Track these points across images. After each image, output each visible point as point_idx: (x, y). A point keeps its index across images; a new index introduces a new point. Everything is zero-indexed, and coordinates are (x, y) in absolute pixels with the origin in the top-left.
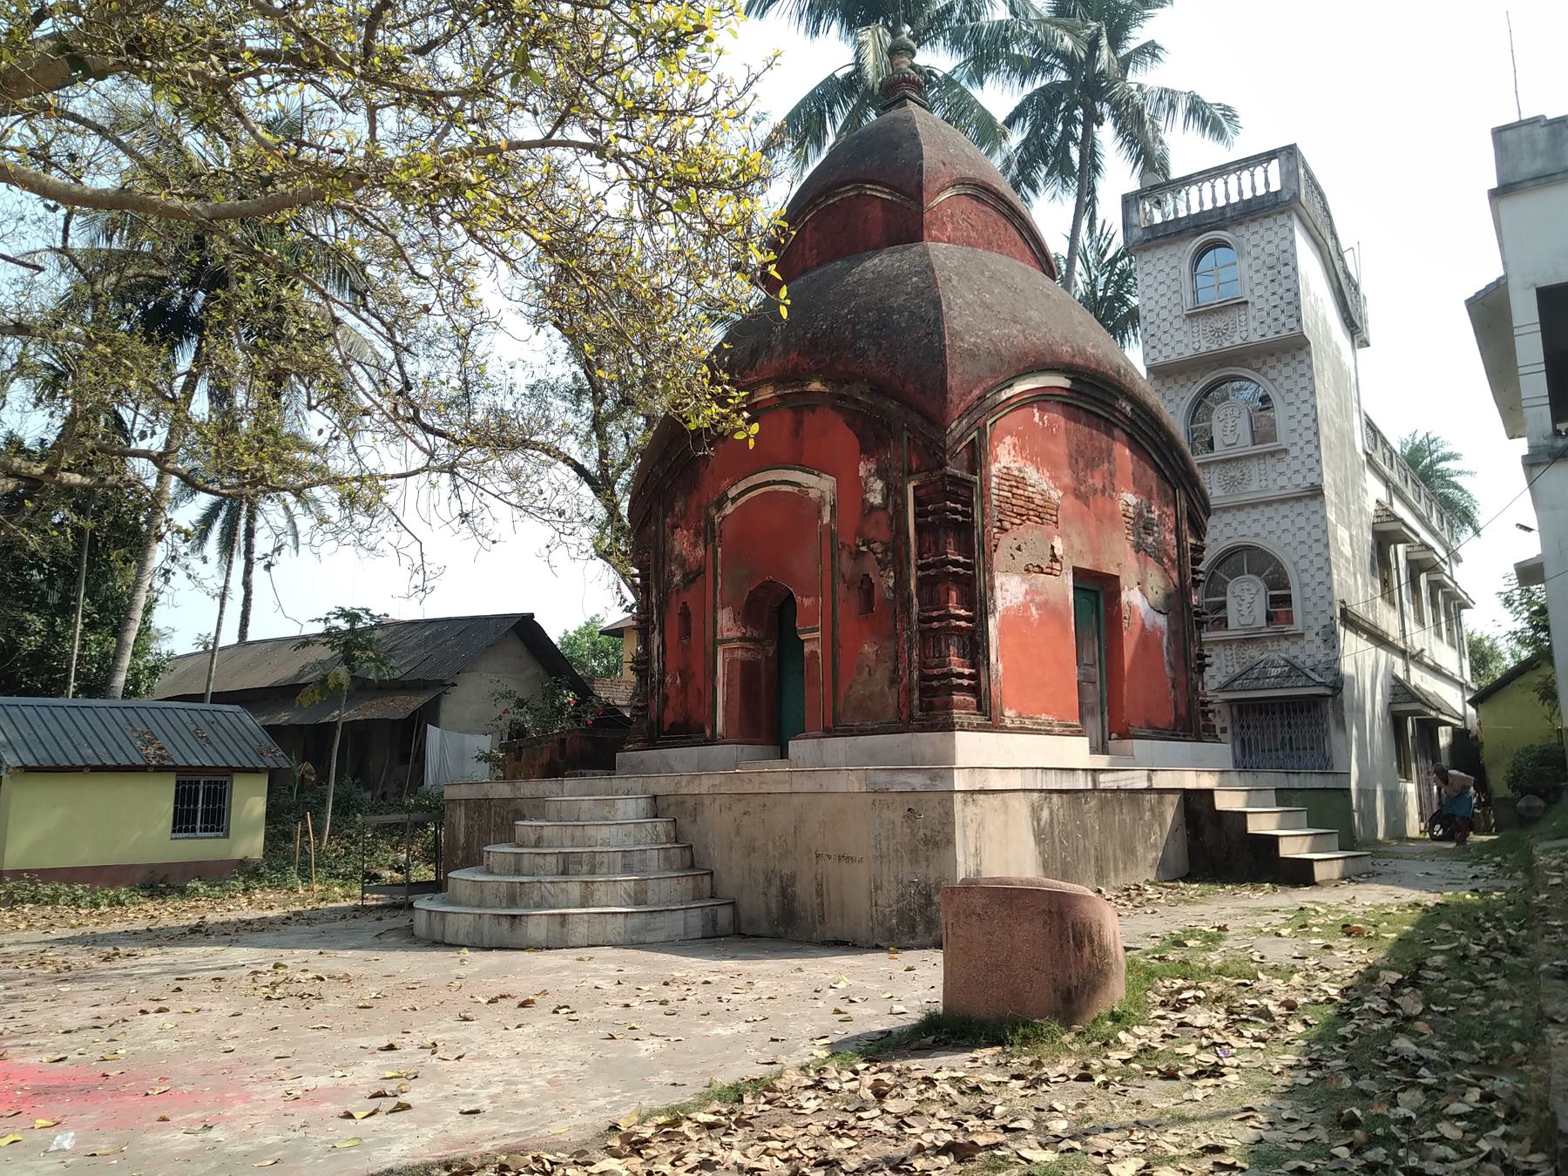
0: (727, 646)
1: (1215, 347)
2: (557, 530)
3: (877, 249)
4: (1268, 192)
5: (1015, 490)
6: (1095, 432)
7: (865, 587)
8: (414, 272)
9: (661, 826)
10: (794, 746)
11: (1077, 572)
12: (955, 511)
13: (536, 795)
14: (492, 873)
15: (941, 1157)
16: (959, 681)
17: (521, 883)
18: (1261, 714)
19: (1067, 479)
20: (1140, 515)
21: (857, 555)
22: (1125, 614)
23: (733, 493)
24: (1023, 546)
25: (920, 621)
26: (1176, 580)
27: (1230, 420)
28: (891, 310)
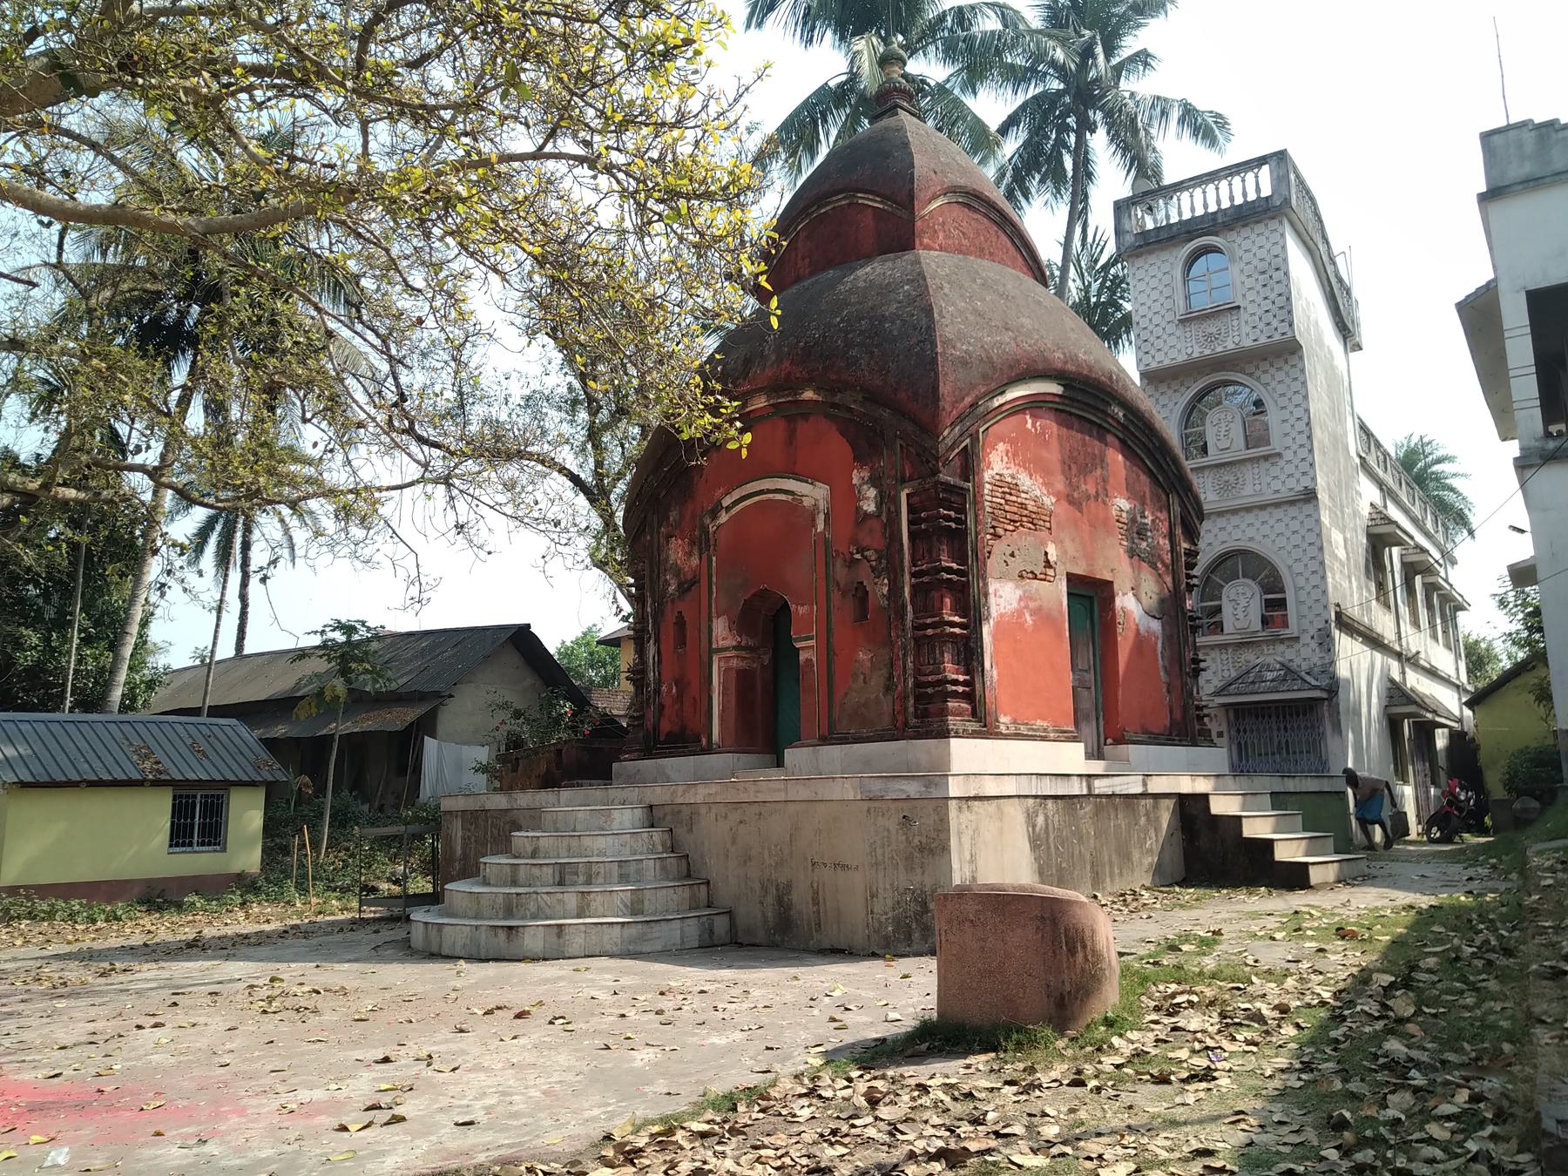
1: (1207, 352)
2: (553, 540)
3: (868, 257)
5: (1008, 497)
7: (860, 594)
8: (407, 285)
9: (657, 836)
10: (790, 755)
11: (1071, 578)
12: (949, 518)
16: (954, 688)
17: (518, 894)
18: (1257, 717)
19: (1060, 484)
20: (1133, 520)
21: (851, 563)
22: (1120, 619)
23: (727, 502)
24: (1016, 553)
25: (915, 628)
26: (1170, 585)
27: (1223, 425)
28: (883, 318)
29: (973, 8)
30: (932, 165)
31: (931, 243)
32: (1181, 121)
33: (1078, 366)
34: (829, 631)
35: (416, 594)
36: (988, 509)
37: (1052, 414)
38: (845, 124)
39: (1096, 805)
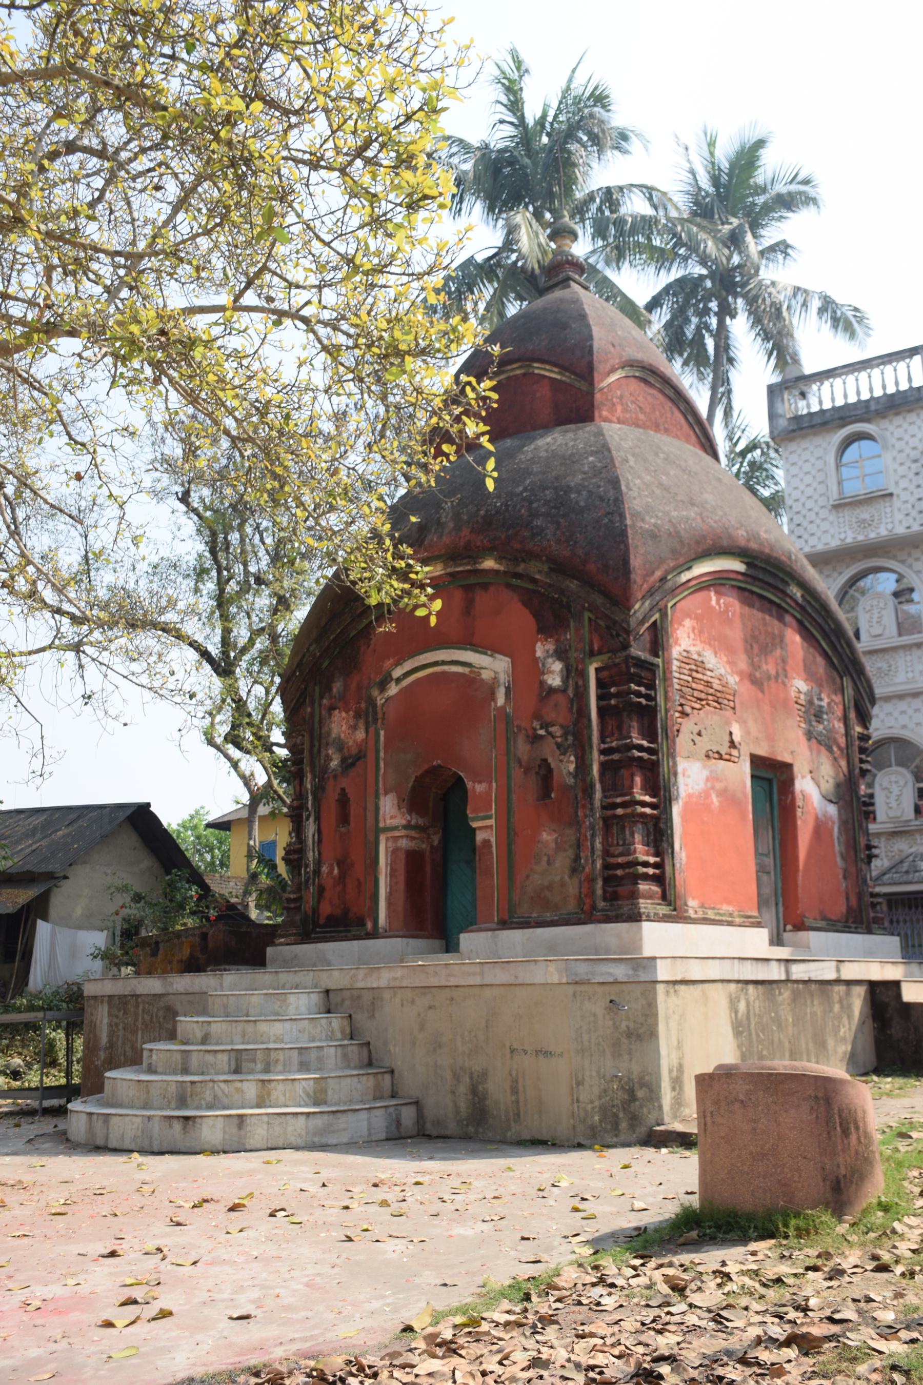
0: (390, 834)
1: (861, 538)
2: (189, 713)
3: (547, 427)
4: (911, 387)
5: (695, 674)
6: (767, 617)
7: (543, 772)
8: (71, 438)
9: (337, 1022)
11: (757, 762)
12: (638, 694)
13: (191, 990)
14: (155, 1072)
15: (785, 1349)
16: (645, 870)
17: (193, 1083)
18: (910, 908)
19: (743, 664)
20: (810, 702)
21: (535, 739)
22: (799, 802)
23: (397, 673)
24: (703, 732)
25: (604, 807)
26: (845, 769)
27: (875, 611)
28: (568, 489)
29: (621, 189)
30: (610, 339)
31: (610, 417)
32: (822, 311)
35: (37, 768)
36: (677, 687)
37: (735, 592)
38: (493, 296)
39: (793, 991)
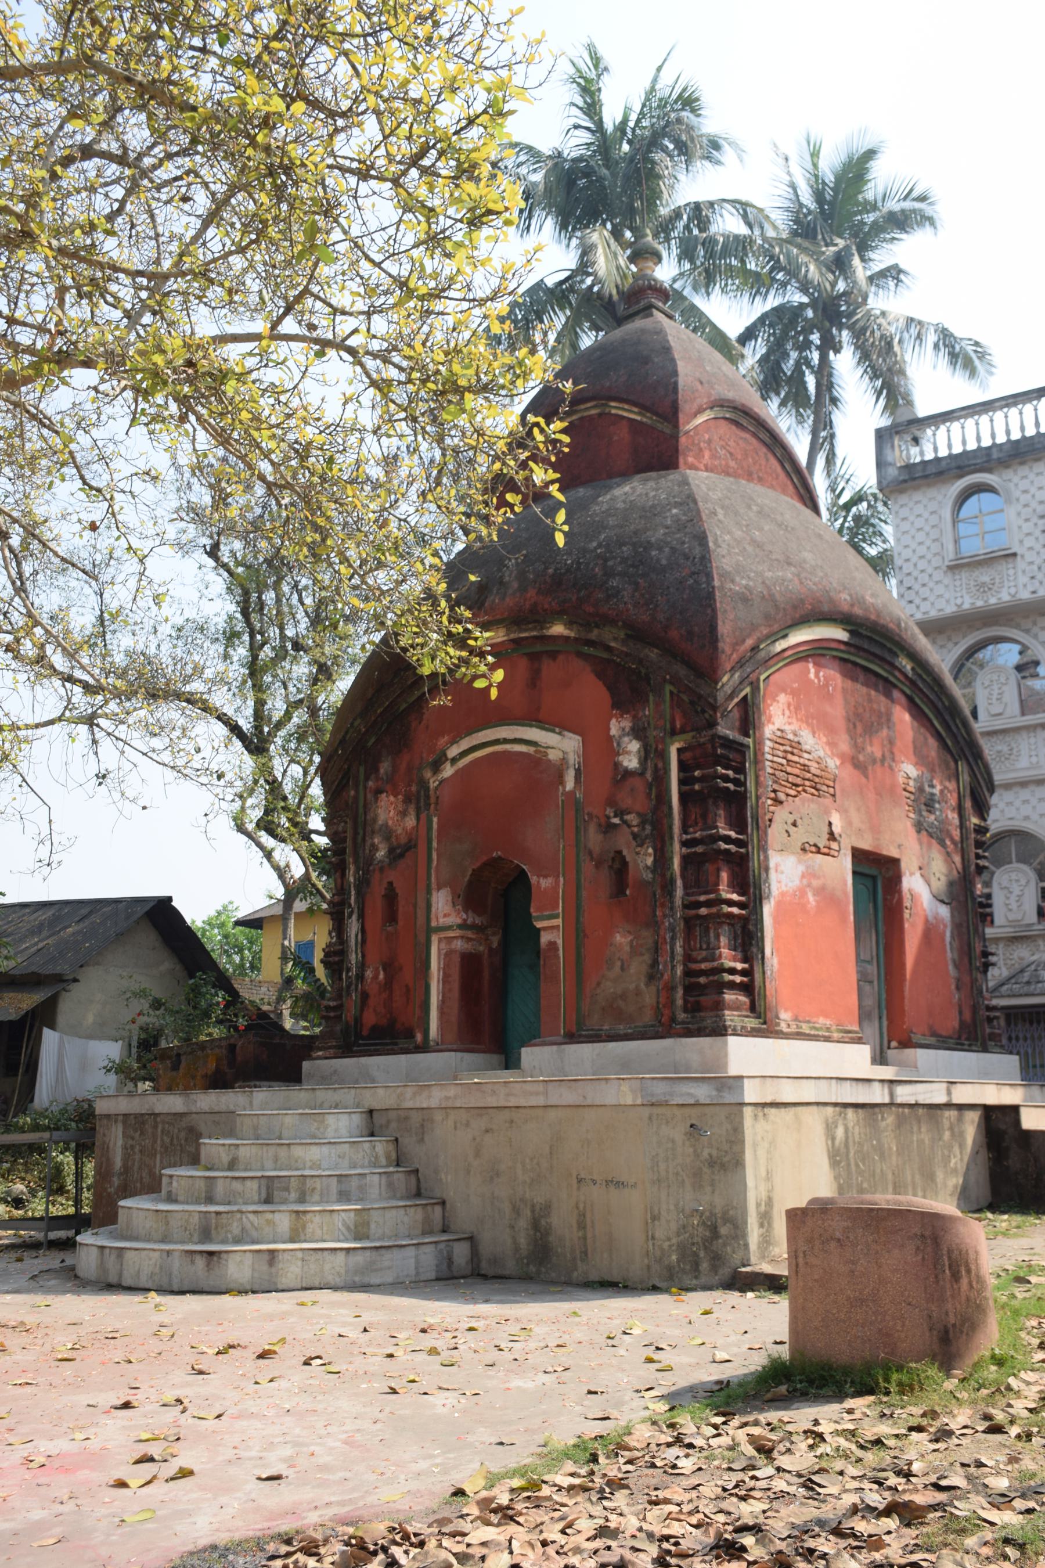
0: (443, 935)
1: (980, 603)
2: (217, 795)
3: (626, 474)
4: (1038, 433)
5: (790, 756)
6: (873, 693)
7: (617, 866)
8: (85, 483)
9: (381, 1147)
10: (528, 1055)
11: (859, 856)
12: (726, 779)
13: (216, 1109)
14: (175, 1201)
16: (731, 977)
17: (218, 1213)
18: (1031, 1023)
19: (845, 745)
20: (921, 789)
21: (608, 828)
22: (907, 903)
23: (453, 752)
24: (799, 822)
25: (686, 906)
26: (959, 865)
27: (995, 687)
28: (648, 546)
29: (711, 204)
30: (697, 374)
33: (866, 610)
34: (578, 907)
38: (565, 326)
39: (898, 1116)
